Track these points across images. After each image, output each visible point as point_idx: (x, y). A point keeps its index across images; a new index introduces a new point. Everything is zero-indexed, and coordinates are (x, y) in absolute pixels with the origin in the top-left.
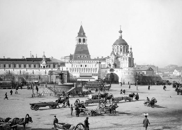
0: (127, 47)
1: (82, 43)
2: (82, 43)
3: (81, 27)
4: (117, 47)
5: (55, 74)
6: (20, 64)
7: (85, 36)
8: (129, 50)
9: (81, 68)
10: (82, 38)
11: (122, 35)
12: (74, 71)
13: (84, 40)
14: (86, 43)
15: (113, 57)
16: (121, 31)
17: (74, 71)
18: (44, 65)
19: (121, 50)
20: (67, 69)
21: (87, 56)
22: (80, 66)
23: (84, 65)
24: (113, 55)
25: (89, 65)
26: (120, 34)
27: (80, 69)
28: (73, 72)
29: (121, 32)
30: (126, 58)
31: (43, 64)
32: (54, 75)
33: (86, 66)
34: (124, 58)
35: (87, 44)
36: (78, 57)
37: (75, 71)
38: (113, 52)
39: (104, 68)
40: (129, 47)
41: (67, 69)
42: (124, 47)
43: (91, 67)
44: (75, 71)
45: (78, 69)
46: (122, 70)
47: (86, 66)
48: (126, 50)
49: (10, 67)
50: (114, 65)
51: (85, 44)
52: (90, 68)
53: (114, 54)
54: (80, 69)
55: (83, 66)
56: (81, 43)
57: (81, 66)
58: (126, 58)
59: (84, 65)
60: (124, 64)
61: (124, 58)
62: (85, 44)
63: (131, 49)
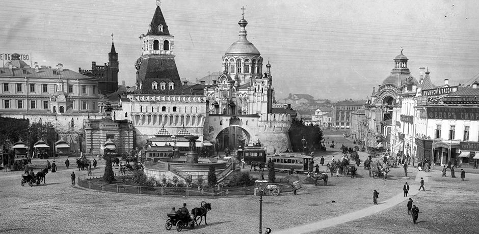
0: (259, 61)
1: (161, 51)
2: (161, 51)
3: (158, 9)
4: (235, 62)
5: (103, 130)
6: (20, 99)
7: (169, 35)
8: (264, 70)
9: (164, 113)
10: (161, 39)
11: (246, 32)
12: (146, 122)
13: (166, 46)
14: (171, 52)
15: (225, 86)
16: (245, 21)
17: (146, 122)
18: (61, 105)
19: (246, 70)
20: (126, 116)
21: (174, 85)
22: (160, 110)
23: (169, 106)
24: (225, 80)
25: (183, 106)
26: (242, 28)
27: (161, 116)
28: (143, 125)
29: (244, 24)
30: (261, 89)
31: (59, 102)
32: (101, 132)
33: (175, 109)
34: (257, 89)
35: (172, 53)
36: (153, 88)
37: (144, 120)
38: (226, 72)
39: (214, 115)
40: (265, 63)
41: (126, 116)
42: (253, 61)
43: (188, 110)
44: (144, 120)
45: (155, 116)
46: (260, 119)
47: (175, 109)
48: (256, 69)
49: (8, 90)
50: (229, 105)
51: (168, 52)
52: (185, 115)
53: (230, 79)
54: (161, 116)
55: (167, 110)
56: (158, 52)
57: (164, 109)
58: (261, 89)
59: (169, 106)
60: (255, 104)
61: (257, 89)
62: (168, 52)
63: (269, 66)
